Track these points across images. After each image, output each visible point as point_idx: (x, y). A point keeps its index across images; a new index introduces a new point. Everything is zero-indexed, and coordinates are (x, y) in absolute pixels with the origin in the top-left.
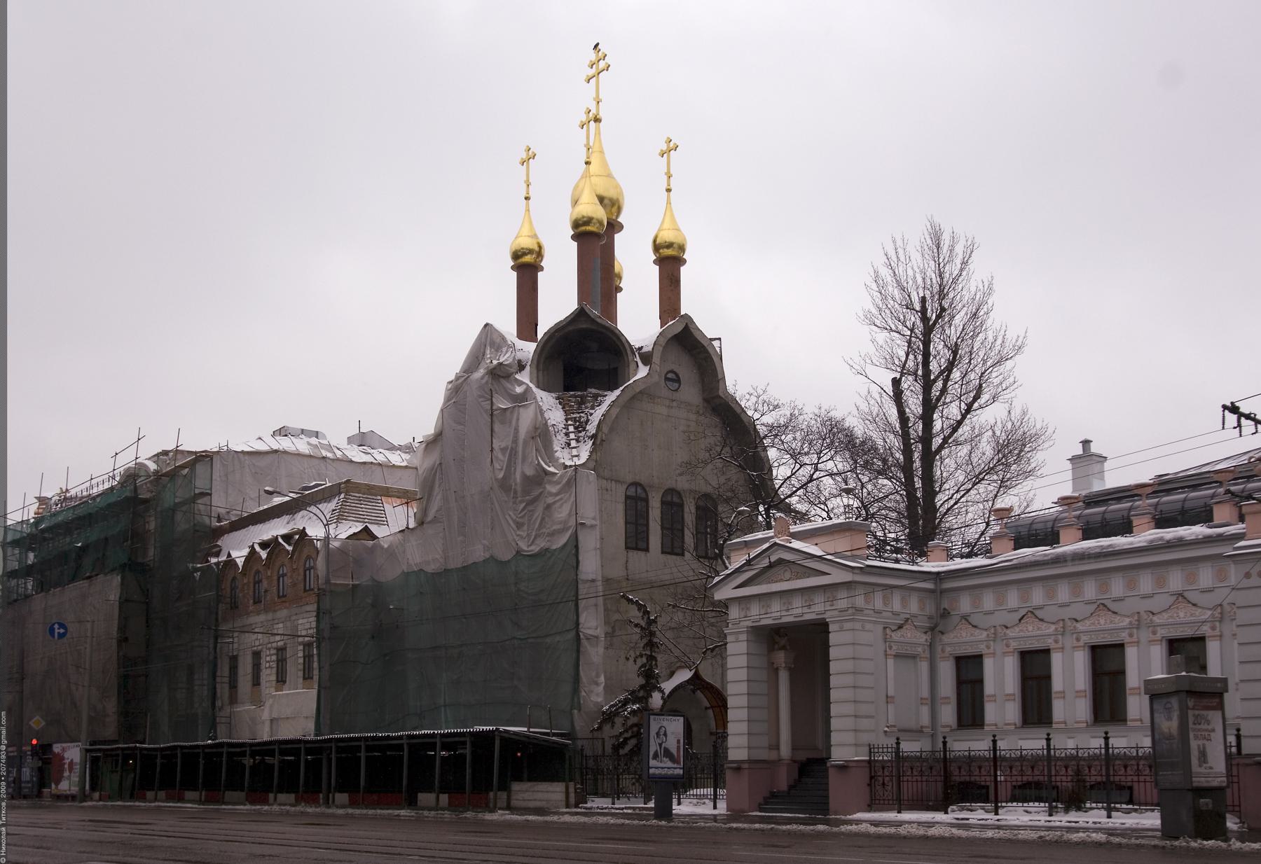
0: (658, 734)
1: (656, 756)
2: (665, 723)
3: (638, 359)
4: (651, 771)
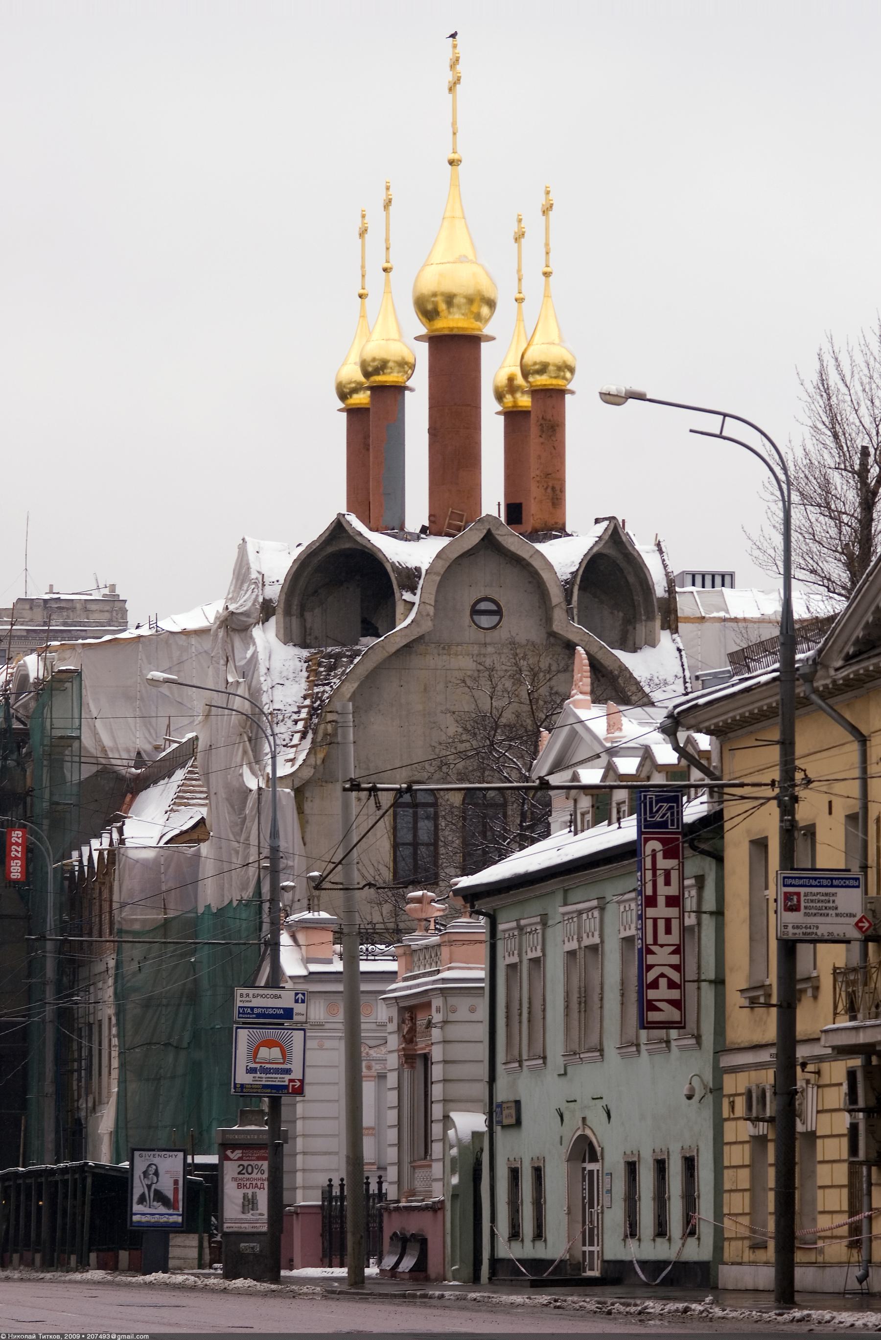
0: (145, 1174)
1: (142, 1200)
2: (156, 1161)
4: (135, 1218)
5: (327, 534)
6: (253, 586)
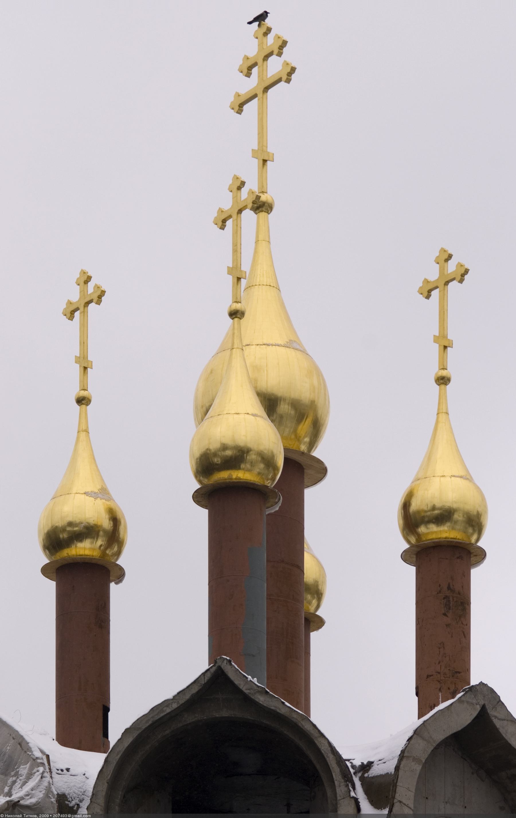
3: (360, 793)
5: (194, 690)
6: (41, 769)
